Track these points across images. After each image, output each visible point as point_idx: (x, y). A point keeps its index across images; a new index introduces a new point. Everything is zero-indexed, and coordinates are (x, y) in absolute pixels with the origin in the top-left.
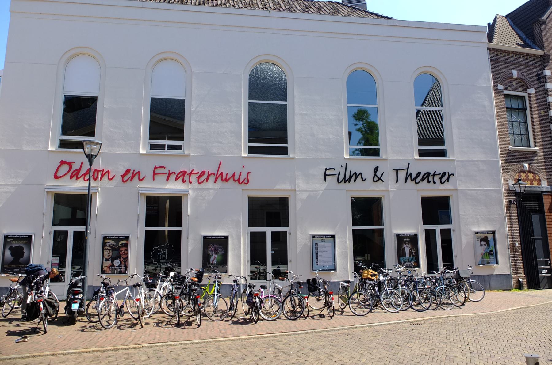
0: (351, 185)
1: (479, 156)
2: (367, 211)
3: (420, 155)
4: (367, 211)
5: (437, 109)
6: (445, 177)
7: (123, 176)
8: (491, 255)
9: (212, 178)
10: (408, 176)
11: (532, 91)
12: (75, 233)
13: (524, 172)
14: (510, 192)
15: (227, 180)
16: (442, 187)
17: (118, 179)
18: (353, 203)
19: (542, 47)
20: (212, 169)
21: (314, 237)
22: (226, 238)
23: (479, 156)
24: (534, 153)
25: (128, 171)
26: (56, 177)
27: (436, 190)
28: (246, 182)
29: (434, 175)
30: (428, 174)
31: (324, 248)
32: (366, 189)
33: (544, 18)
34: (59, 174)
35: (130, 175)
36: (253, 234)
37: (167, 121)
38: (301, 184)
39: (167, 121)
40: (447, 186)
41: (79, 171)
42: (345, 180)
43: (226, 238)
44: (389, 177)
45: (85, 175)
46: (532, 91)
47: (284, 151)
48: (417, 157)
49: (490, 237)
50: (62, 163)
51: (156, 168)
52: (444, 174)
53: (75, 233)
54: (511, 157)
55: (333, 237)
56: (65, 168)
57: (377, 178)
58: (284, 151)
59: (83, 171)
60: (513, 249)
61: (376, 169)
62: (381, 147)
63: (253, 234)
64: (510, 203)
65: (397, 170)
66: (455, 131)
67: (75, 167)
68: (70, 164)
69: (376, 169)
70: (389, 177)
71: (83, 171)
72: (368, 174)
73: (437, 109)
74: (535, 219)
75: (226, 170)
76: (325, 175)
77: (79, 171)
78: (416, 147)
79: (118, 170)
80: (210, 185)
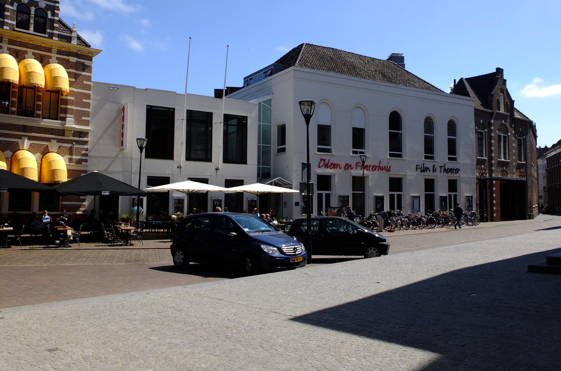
0: (425, 173)
1: (469, 162)
2: (429, 185)
3: (318, 151)
4: (429, 185)
5: (454, 137)
6: (457, 171)
7: (345, 167)
8: (470, 207)
9: (377, 168)
10: (445, 169)
11: (486, 130)
12: (326, 194)
13: (482, 169)
14: (477, 179)
15: (382, 170)
16: (455, 175)
17: (343, 168)
18: (225, 182)
19: (491, 109)
20: (377, 165)
21: (413, 197)
22: (383, 197)
23: (469, 162)
24: (485, 160)
25: (346, 164)
26: (319, 167)
27: (453, 176)
28: (389, 170)
29: (370, 166)
30: (451, 169)
31: (416, 201)
32: (429, 175)
33: (493, 93)
34: (321, 165)
35: (348, 167)
36: (390, 195)
37: (358, 138)
38: (408, 173)
39: (358, 138)
40: (457, 175)
41: (328, 164)
42: (424, 171)
43: (383, 197)
44: (438, 170)
45: (330, 166)
46: (486, 130)
47: (400, 156)
48: (351, 154)
49: (470, 199)
50: (321, 160)
51: (357, 163)
52: (374, 166)
53: (326, 194)
54: (480, 162)
55: (419, 197)
56: (322, 163)
57: (434, 170)
58: (400, 156)
59: (329, 165)
60: (477, 204)
61: (434, 166)
62: (332, 147)
63: (390, 195)
64: (477, 183)
65: (441, 167)
66: (461, 149)
67: (327, 162)
68: (324, 160)
69: (434, 166)
70: (438, 170)
71: (329, 165)
72: (431, 169)
73: (454, 137)
74: (484, 190)
75: (382, 165)
76: (417, 168)
77: (328, 164)
78: (388, 152)
79: (343, 164)
80: (376, 172)
